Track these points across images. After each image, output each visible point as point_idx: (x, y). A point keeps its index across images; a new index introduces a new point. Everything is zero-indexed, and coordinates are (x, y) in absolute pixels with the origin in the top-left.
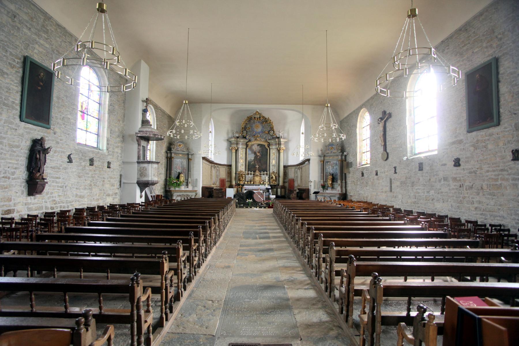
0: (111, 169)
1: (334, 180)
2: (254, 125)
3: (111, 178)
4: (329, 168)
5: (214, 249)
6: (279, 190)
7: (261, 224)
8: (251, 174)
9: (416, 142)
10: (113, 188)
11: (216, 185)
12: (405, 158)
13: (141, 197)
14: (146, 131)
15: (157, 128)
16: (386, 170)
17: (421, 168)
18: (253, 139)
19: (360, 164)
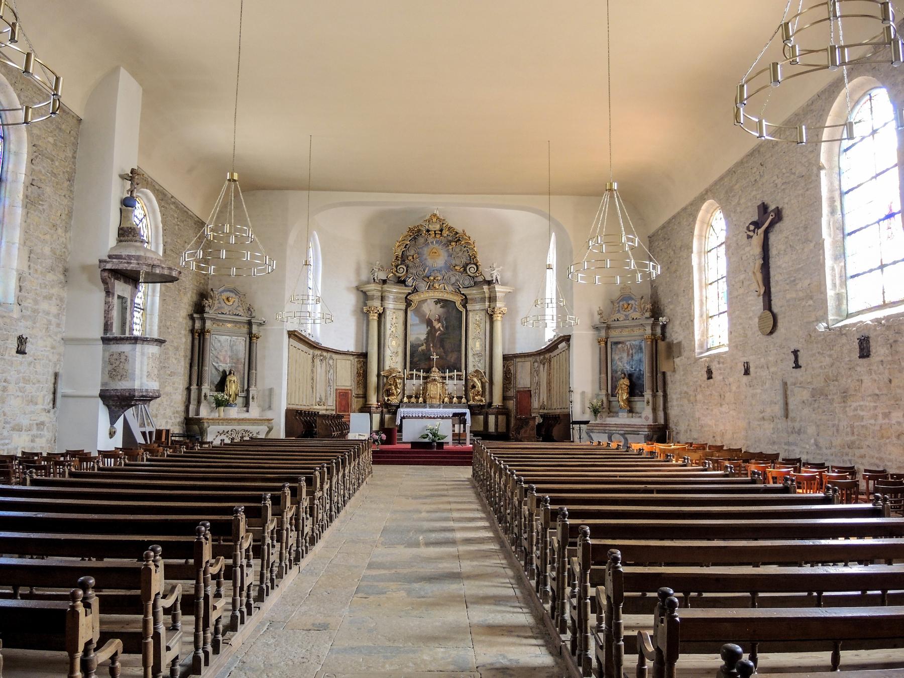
0: (27, 358)
1: (635, 389)
2: (426, 250)
3: (27, 381)
4: (620, 359)
5: (291, 577)
6: (492, 419)
7: (434, 507)
8: (418, 377)
9: (850, 282)
10: (32, 408)
11: (328, 406)
12: (822, 327)
13: (112, 434)
14: (129, 257)
15: (165, 252)
16: (771, 357)
17: (865, 350)
18: (423, 286)
19: (701, 346)
